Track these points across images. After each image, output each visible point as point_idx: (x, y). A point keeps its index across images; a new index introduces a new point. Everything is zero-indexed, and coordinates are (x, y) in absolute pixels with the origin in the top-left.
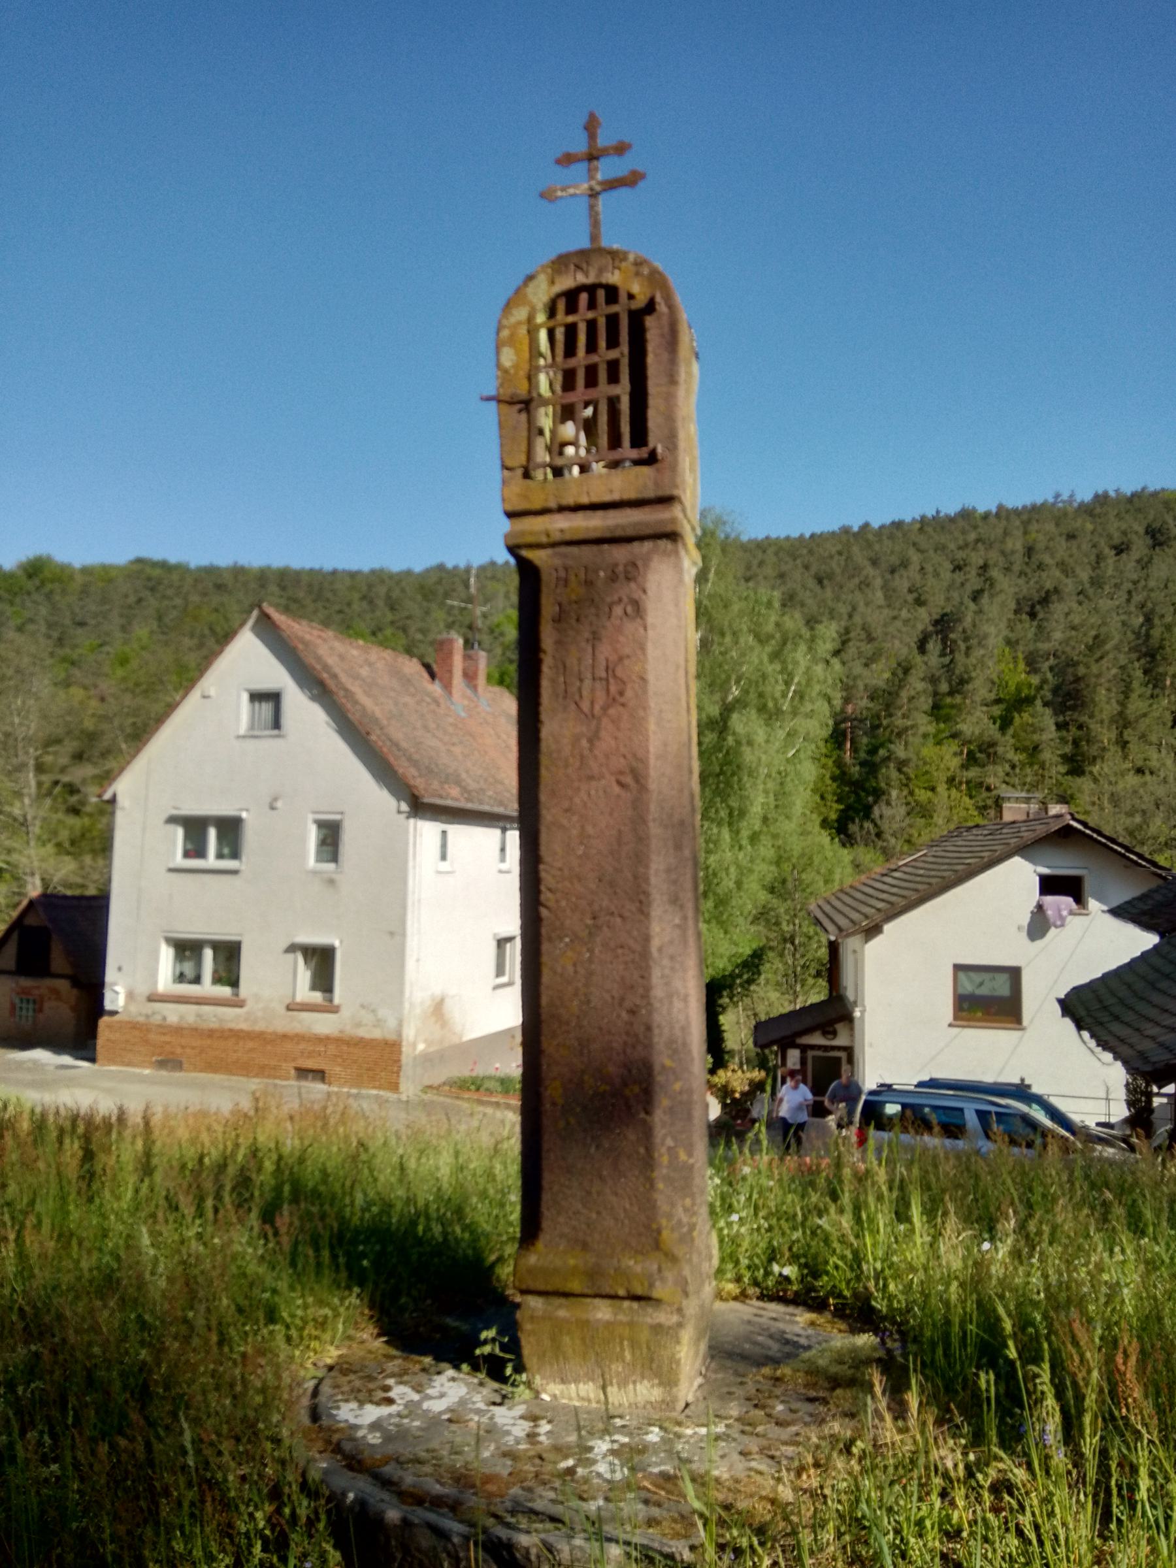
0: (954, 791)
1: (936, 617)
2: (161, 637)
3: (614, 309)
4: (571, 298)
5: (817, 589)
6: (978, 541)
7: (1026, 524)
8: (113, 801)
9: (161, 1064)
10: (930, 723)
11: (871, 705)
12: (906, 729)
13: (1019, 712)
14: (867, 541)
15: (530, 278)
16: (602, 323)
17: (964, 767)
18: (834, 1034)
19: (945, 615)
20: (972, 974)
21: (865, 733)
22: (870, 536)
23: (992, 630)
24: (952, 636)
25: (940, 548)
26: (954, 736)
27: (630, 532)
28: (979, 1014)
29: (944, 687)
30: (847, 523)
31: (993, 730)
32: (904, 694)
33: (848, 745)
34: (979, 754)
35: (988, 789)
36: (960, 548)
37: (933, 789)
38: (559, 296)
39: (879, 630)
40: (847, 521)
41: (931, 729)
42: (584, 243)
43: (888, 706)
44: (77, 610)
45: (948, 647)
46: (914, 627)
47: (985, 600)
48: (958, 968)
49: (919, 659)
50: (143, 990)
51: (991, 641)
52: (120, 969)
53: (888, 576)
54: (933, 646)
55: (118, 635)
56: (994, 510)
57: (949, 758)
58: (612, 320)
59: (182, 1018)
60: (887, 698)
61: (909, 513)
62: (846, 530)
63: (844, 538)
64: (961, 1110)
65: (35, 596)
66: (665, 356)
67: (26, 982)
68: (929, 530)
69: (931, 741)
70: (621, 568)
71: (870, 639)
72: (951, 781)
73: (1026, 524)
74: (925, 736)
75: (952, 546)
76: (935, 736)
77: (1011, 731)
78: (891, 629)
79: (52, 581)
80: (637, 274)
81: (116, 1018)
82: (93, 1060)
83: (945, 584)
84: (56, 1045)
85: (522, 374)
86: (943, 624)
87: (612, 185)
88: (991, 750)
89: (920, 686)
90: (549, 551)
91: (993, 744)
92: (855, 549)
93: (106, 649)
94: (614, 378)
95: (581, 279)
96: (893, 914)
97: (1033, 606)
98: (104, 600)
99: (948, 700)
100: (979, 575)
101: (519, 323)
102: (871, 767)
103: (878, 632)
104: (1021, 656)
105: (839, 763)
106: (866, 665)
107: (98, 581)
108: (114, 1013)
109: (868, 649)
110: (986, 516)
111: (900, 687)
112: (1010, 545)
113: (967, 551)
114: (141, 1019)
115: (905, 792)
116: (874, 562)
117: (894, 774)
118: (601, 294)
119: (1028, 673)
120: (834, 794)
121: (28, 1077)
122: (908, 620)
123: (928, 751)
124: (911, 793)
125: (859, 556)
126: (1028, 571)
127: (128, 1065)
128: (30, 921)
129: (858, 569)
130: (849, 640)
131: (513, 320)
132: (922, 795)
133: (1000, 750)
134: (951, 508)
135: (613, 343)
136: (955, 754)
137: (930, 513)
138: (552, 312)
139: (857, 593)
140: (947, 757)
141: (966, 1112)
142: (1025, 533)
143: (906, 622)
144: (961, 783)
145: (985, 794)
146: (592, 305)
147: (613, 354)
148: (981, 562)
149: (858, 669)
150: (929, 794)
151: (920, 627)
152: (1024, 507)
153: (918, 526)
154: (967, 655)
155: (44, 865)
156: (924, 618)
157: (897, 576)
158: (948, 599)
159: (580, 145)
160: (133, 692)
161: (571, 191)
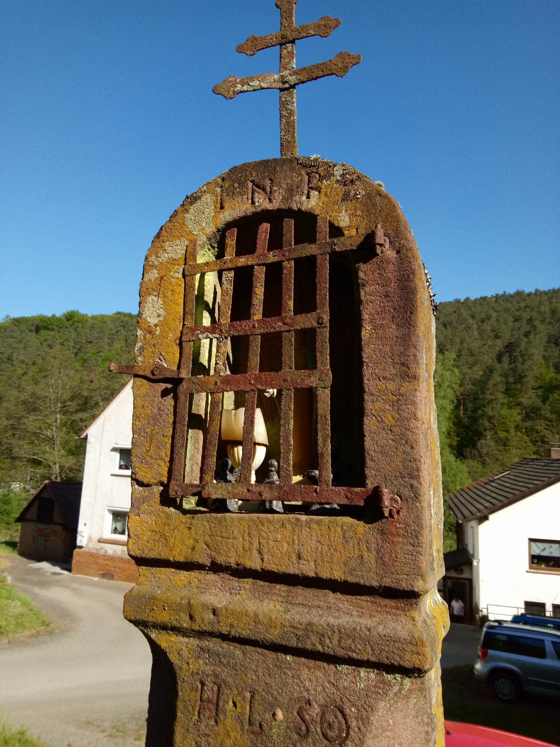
0: (519, 433)
1: (505, 344)
2: (126, 349)
3: (310, 250)
4: (244, 231)
5: (444, 329)
6: (526, 307)
7: (550, 298)
8: (86, 438)
9: (104, 576)
10: (505, 398)
11: (473, 388)
12: (492, 400)
13: (552, 393)
14: (468, 306)
15: (192, 199)
16: (289, 267)
17: (524, 420)
18: (462, 571)
19: (511, 343)
20: (538, 544)
21: (470, 402)
22: (470, 304)
23: (536, 351)
24: (514, 354)
25: (507, 310)
26: (518, 404)
27: (331, 646)
28: (543, 566)
29: (511, 380)
30: (458, 297)
31: (538, 402)
32: (491, 383)
33: (462, 408)
34: (531, 413)
35: (537, 432)
36: (517, 310)
37: (507, 431)
38: (229, 225)
39: (477, 351)
40: (458, 297)
41: (505, 401)
42: (273, 152)
43: (482, 389)
44: (88, 336)
45: (513, 360)
46: (494, 349)
47: (532, 336)
48: (531, 540)
49: (498, 366)
50: (96, 536)
51: (535, 357)
52: (85, 525)
53: (480, 324)
54: (505, 359)
55: (107, 347)
56: (533, 292)
57: (515, 416)
58: (306, 266)
59: (114, 552)
60: (482, 384)
61: (489, 293)
62: (457, 301)
63: (457, 305)
64: (543, 641)
65: (71, 330)
66: (392, 331)
67: (41, 526)
68: (501, 301)
69: (505, 407)
70: (315, 711)
71: (472, 355)
72: (517, 427)
73: (550, 298)
74: (503, 404)
75: (513, 309)
76: (508, 405)
77: (548, 403)
78: (482, 350)
79: (78, 322)
80: (346, 197)
81: (82, 550)
82: (70, 570)
83: (510, 328)
84: (54, 561)
85: (173, 336)
86: (510, 348)
87: (311, 75)
88: (538, 412)
89: (499, 379)
90: (194, 642)
91: (539, 409)
92: (463, 310)
93: (101, 354)
94: (307, 361)
95: (262, 202)
96: (495, 509)
97: (556, 340)
98: (101, 332)
99: (514, 386)
100: (528, 324)
101: (173, 261)
102: (474, 419)
103: (476, 351)
104: (551, 364)
105: (457, 417)
106: (470, 368)
107: (100, 322)
108: (81, 547)
109: (471, 360)
110: (529, 295)
111: (489, 379)
112: (543, 309)
113: (521, 312)
114: (94, 551)
115: (493, 433)
116: (473, 317)
117: (487, 423)
118: (289, 225)
119: (556, 373)
120: (455, 432)
121: (36, 579)
122: (491, 346)
123: (505, 412)
124: (496, 433)
125: (465, 313)
126: (553, 322)
127: (87, 575)
128: (44, 495)
129: (465, 320)
130: (461, 355)
131: (164, 257)
132: (502, 435)
133: (543, 412)
134: (511, 290)
135: (306, 303)
136: (519, 414)
137: (501, 293)
138: (220, 246)
139: (465, 332)
140: (515, 415)
141: (546, 643)
142: (550, 303)
143: (490, 346)
144: (522, 428)
145: (535, 435)
146: (275, 243)
147: (306, 321)
148: (528, 317)
149: (466, 370)
150: (506, 433)
151: (498, 349)
152: (549, 290)
153: (494, 299)
154: (523, 364)
155: (60, 460)
156: (499, 344)
157: (485, 324)
158: (512, 336)
159: (271, 28)
160: (106, 378)
161: (256, 83)
